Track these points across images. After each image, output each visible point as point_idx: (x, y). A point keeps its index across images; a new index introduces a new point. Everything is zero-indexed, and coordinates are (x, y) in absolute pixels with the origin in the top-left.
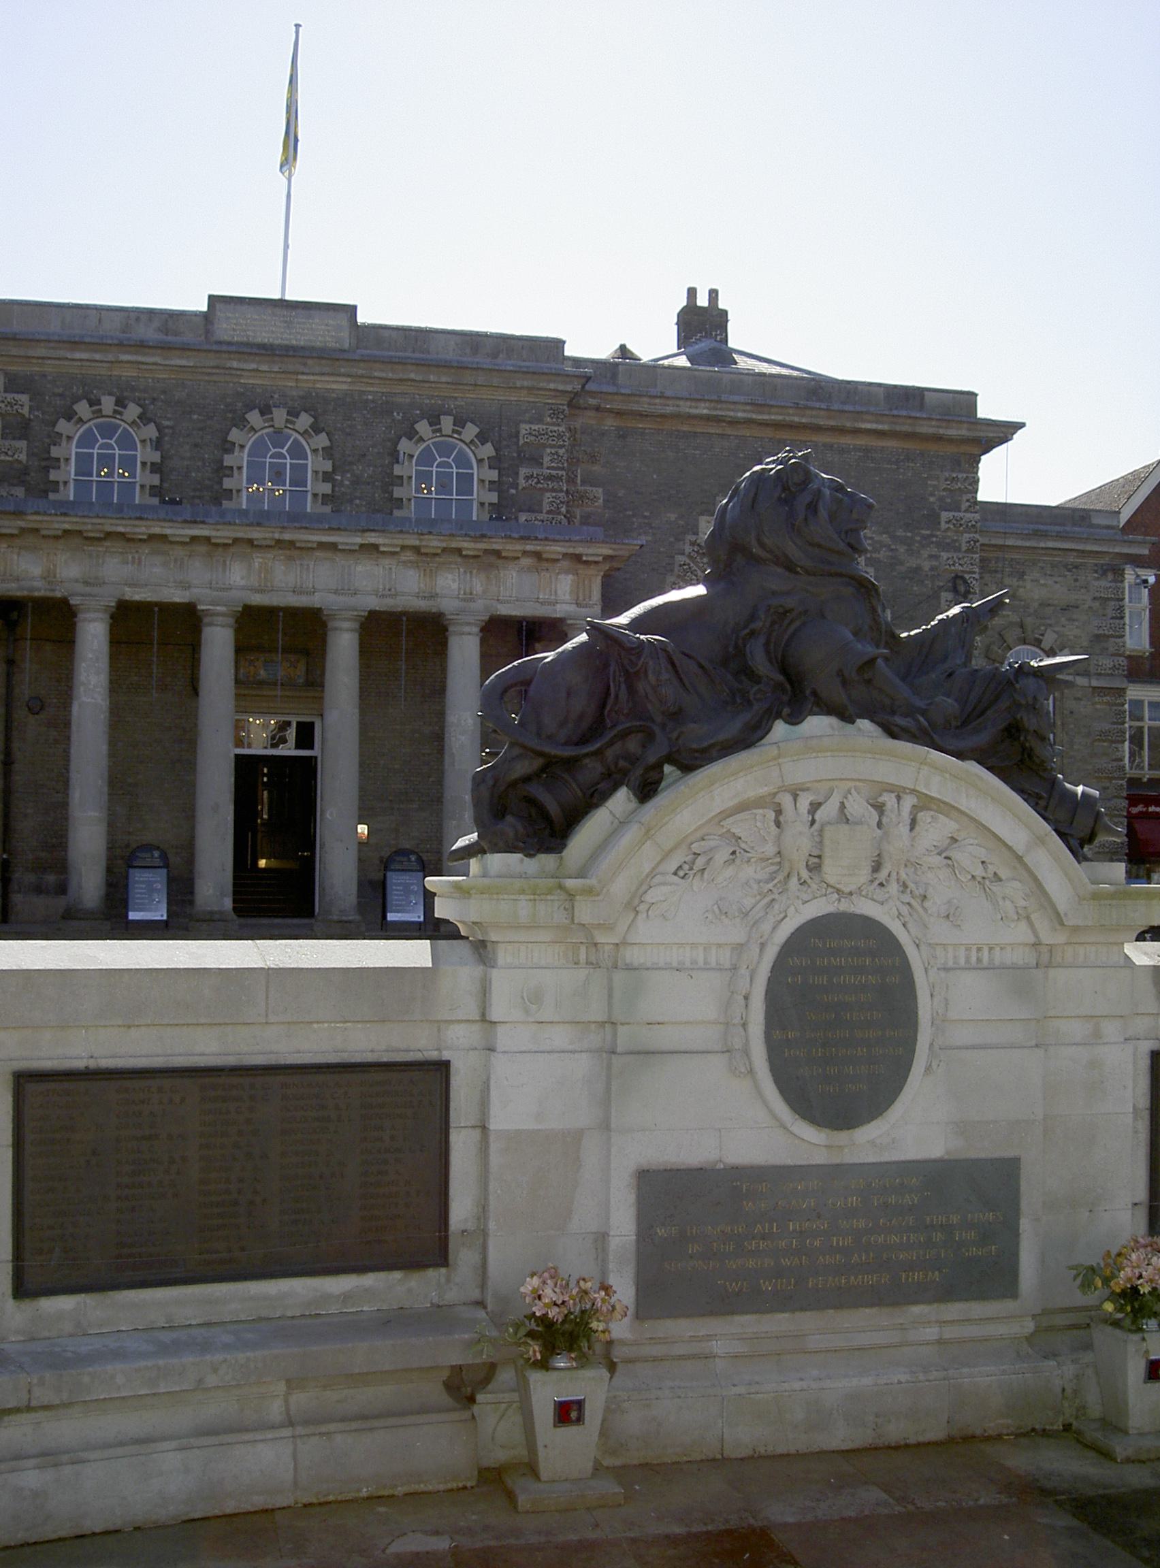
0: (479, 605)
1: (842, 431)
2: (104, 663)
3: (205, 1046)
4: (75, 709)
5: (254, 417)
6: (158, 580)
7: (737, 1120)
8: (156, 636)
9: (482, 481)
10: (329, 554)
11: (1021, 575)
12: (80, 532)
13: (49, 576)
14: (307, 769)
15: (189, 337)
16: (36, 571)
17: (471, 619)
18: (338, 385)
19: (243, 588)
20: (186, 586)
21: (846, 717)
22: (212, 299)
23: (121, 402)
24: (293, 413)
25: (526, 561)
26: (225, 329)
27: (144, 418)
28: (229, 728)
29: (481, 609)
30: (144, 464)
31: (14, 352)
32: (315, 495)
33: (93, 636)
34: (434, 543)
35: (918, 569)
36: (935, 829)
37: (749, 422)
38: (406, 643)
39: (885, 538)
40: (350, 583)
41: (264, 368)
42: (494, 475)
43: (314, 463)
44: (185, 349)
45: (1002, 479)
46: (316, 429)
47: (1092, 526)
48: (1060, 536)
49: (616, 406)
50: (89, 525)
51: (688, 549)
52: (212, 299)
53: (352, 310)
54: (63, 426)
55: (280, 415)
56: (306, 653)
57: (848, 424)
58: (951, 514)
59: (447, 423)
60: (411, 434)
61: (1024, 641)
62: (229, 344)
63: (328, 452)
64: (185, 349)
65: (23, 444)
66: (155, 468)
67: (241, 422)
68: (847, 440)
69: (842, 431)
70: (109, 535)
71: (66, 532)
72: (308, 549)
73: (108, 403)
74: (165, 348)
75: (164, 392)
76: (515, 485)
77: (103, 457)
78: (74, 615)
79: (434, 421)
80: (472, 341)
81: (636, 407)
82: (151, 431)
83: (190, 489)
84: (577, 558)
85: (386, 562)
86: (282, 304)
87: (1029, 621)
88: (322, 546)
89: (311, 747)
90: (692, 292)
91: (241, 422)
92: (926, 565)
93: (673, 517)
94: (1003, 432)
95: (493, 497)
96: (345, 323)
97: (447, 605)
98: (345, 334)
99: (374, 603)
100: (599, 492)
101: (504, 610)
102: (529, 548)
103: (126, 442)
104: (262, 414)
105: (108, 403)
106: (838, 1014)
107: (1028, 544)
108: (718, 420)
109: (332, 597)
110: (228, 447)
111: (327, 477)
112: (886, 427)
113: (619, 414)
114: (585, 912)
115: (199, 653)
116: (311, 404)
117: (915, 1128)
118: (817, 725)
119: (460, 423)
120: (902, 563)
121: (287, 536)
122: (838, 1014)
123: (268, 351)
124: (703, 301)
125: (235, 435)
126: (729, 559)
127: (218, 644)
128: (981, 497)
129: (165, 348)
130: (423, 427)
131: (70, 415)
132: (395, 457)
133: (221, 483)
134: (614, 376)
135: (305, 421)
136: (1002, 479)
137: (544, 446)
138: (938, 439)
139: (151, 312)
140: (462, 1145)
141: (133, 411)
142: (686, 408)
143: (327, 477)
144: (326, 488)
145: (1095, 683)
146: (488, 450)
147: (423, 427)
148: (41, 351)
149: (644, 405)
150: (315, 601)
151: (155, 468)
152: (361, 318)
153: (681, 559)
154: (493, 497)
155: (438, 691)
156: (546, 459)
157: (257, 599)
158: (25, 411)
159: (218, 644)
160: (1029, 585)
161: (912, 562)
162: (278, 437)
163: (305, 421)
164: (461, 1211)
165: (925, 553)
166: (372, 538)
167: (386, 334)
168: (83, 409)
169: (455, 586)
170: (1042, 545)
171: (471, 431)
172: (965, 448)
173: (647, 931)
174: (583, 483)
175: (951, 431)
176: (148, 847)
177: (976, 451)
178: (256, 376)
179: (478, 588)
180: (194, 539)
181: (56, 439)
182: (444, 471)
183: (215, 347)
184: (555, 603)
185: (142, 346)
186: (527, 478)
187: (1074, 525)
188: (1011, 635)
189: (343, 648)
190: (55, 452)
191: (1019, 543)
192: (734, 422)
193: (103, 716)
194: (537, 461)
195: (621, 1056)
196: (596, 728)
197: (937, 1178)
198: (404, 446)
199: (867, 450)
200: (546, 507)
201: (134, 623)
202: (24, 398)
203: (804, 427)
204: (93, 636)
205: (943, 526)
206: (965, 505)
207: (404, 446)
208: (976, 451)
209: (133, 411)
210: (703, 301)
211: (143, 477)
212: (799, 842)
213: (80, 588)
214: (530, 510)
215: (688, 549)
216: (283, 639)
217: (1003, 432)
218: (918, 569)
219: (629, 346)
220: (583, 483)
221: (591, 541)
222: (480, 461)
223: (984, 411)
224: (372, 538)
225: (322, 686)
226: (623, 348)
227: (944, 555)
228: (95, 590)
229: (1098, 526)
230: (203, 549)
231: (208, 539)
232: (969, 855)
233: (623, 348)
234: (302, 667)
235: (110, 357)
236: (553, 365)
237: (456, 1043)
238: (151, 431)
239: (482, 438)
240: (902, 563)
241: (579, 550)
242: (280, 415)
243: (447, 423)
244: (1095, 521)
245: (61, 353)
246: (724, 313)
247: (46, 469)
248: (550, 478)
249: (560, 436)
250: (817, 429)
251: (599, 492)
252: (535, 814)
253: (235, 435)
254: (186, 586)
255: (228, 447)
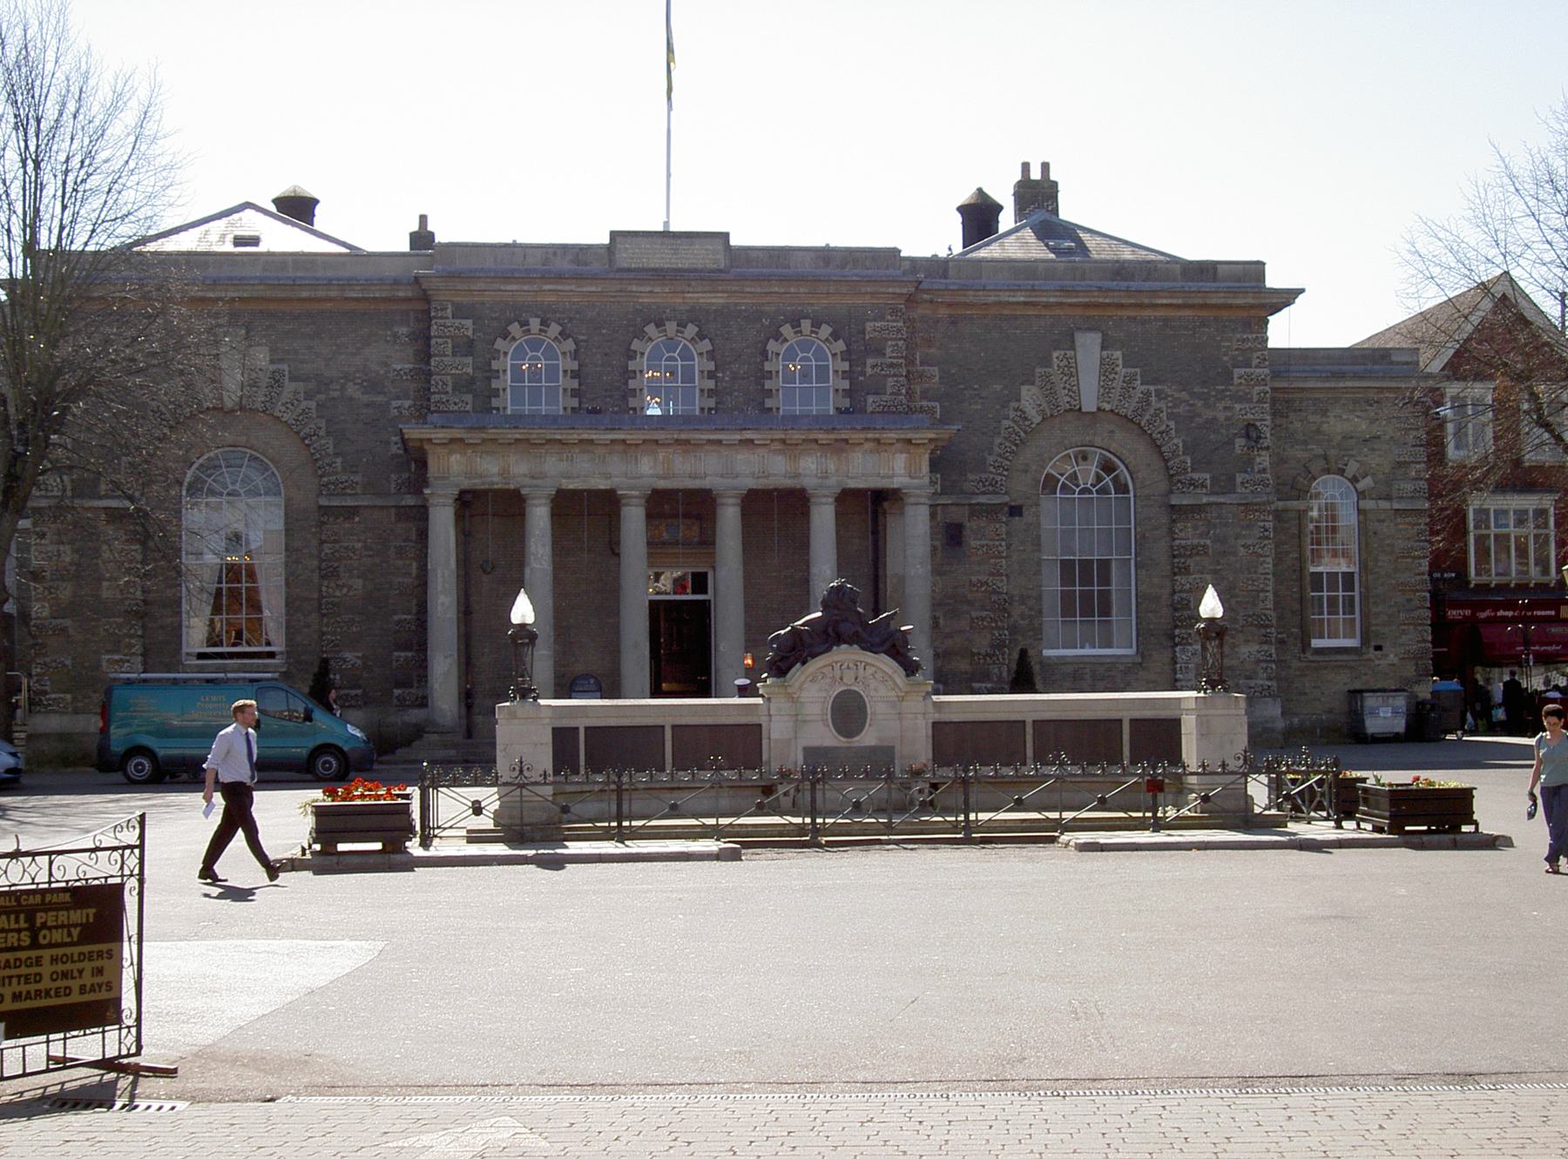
0: (833, 481)
1: (1141, 306)
2: (548, 539)
3: (709, 721)
4: (527, 571)
5: (651, 329)
6: (587, 474)
7: (824, 735)
8: (587, 515)
9: (836, 372)
10: (714, 447)
11: (1324, 413)
12: (528, 440)
13: (504, 473)
14: (703, 610)
15: (596, 267)
16: (495, 470)
17: (826, 492)
18: (718, 300)
19: (652, 476)
20: (608, 476)
21: (850, 644)
22: (613, 234)
23: (545, 323)
24: (682, 325)
25: (868, 446)
26: (624, 259)
27: (564, 334)
28: (644, 583)
29: (835, 483)
30: (565, 372)
31: (459, 287)
32: (702, 391)
33: (539, 517)
34: (797, 436)
35: (1215, 419)
36: (870, 670)
37: (1060, 304)
38: (775, 512)
39: (1184, 395)
40: (733, 468)
41: (657, 289)
42: (846, 366)
43: (700, 364)
44: (594, 278)
45: (1284, 332)
46: (701, 336)
47: (1392, 363)
48: (1357, 376)
49: (948, 299)
50: (535, 434)
51: (1012, 414)
52: (613, 234)
53: (727, 235)
54: (500, 344)
55: (671, 327)
56: (699, 517)
57: (1146, 301)
58: (1242, 371)
59: (806, 325)
60: (778, 336)
61: (1328, 471)
62: (629, 270)
63: (711, 355)
64: (594, 278)
65: (470, 360)
66: (575, 375)
67: (640, 334)
68: (1147, 313)
69: (1141, 306)
70: (549, 441)
71: (517, 440)
72: (698, 445)
73: (535, 323)
74: (578, 278)
75: (578, 312)
76: (863, 373)
77: (533, 371)
78: (524, 501)
79: (796, 324)
80: (826, 255)
81: (963, 299)
82: (570, 345)
83: (603, 399)
84: (909, 441)
85: (760, 451)
86: (666, 234)
87: (1332, 453)
88: (710, 442)
89: (705, 592)
90: (1026, 167)
91: (640, 334)
92: (1221, 416)
93: (998, 387)
94: (1287, 298)
95: (846, 385)
96: (720, 247)
97: (808, 482)
98: (721, 257)
99: (751, 483)
100: (935, 370)
101: (852, 484)
102: (870, 436)
103: (550, 354)
104: (657, 326)
105: (535, 323)
106: (849, 713)
107: (1327, 385)
108: (1033, 304)
109: (720, 480)
110: (631, 355)
111: (711, 375)
112: (1180, 301)
113: (950, 305)
114: (790, 690)
115: (619, 529)
116: (694, 315)
117: (868, 738)
118: (844, 646)
119: (816, 324)
120: (1200, 416)
121: (683, 436)
122: (849, 713)
123: (660, 275)
124: (1036, 174)
125: (636, 345)
126: (826, 606)
127: (634, 520)
128: (1272, 343)
129: (578, 278)
130: (786, 330)
131: (505, 335)
132: (764, 354)
133: (626, 384)
134: (946, 270)
135: (691, 330)
136: (1284, 332)
137: (887, 340)
138: (1230, 307)
139: (565, 248)
140: (765, 742)
141: (555, 329)
142: (1005, 297)
143: (711, 375)
144: (711, 384)
145: (1396, 506)
146: (840, 346)
147: (786, 330)
148: (480, 285)
149: (971, 297)
150: (705, 484)
151: (575, 375)
152: (733, 242)
153: (1006, 423)
154: (846, 385)
155: (803, 545)
156: (888, 350)
157: (662, 484)
158: (470, 333)
159: (634, 520)
160: (1332, 420)
161: (1209, 414)
162: (671, 344)
163: (691, 330)
164: (765, 757)
165: (1220, 406)
166: (748, 435)
167: (755, 254)
168: (515, 328)
169: (813, 467)
170: (1341, 385)
171: (826, 331)
172: (1252, 312)
173: (804, 694)
174: (922, 364)
175: (1244, 294)
176: (587, 676)
177: (1263, 314)
178: (649, 295)
179: (832, 467)
180: (613, 441)
181: (495, 355)
182: (805, 373)
183: (618, 276)
184: (893, 476)
185: (560, 277)
186: (873, 367)
187: (1375, 363)
188: (1315, 467)
189: (729, 518)
190: (495, 365)
191: (1319, 385)
192: (1047, 306)
193: (549, 578)
194: (880, 352)
195: (798, 721)
196: (794, 649)
197: (873, 749)
198: (772, 346)
199: (1166, 320)
200: (889, 391)
201: (567, 505)
202: (469, 323)
203: (1109, 305)
204: (539, 517)
205: (1236, 381)
206: (1255, 362)
207: (772, 346)
208: (1263, 314)
209: (555, 329)
210: (1036, 174)
211: (564, 382)
212: (838, 673)
213: (527, 481)
214: (877, 393)
215: (1012, 414)
216: (683, 513)
217: (1287, 298)
218: (1215, 419)
219: (986, 190)
220: (922, 364)
221: (917, 429)
222: (834, 355)
223: (1273, 281)
224: (748, 435)
225: (713, 543)
226: (980, 190)
227: (1238, 407)
228: (539, 482)
229: (1398, 363)
230: (620, 448)
231: (624, 441)
232: (879, 675)
233: (980, 190)
234: (696, 528)
235: (535, 287)
236: (890, 271)
237: (763, 720)
238: (570, 345)
239: (835, 336)
240: (1200, 416)
241: (909, 436)
242: (671, 327)
243: (806, 325)
244: (1394, 358)
245: (497, 286)
246: (1055, 184)
247: (489, 379)
248: (892, 365)
249: (899, 331)
250: (1121, 306)
251: (935, 370)
252: (780, 668)
253: (636, 345)
254: (608, 476)
255: (631, 355)
